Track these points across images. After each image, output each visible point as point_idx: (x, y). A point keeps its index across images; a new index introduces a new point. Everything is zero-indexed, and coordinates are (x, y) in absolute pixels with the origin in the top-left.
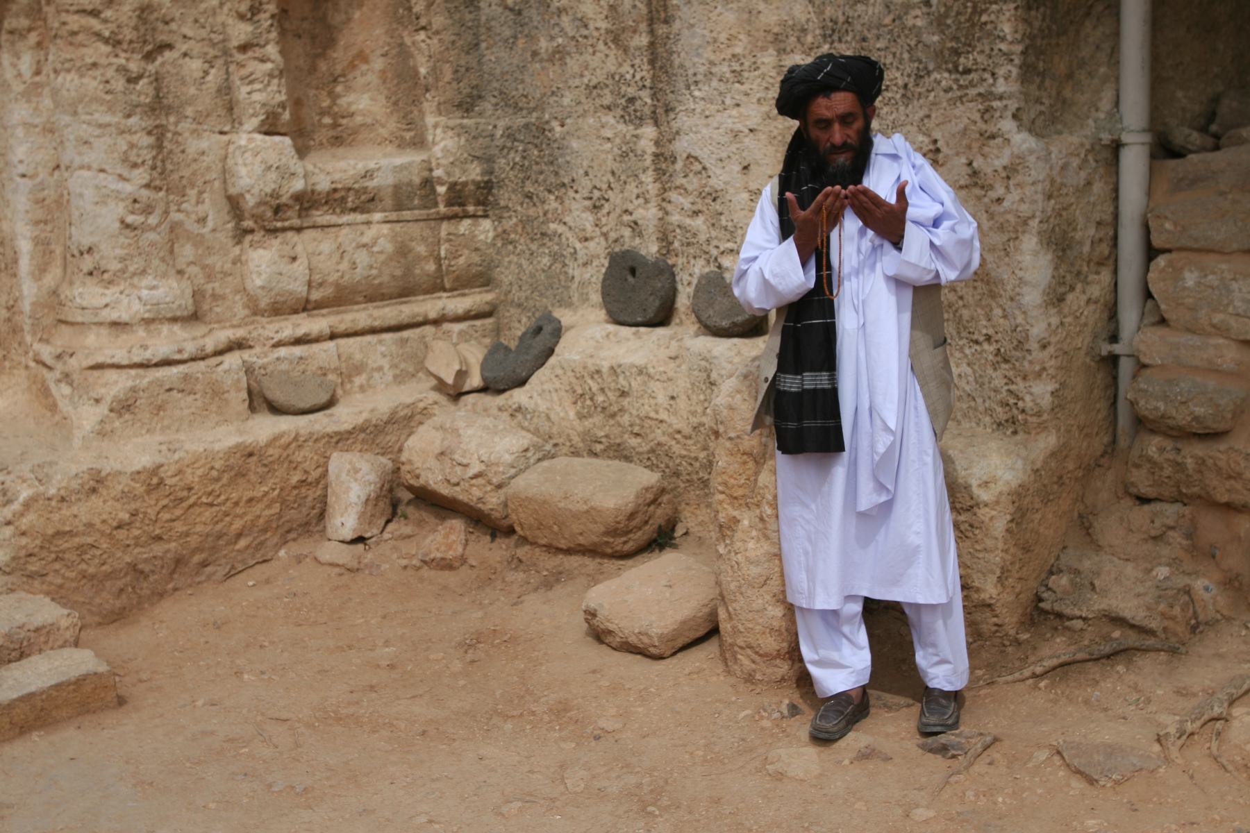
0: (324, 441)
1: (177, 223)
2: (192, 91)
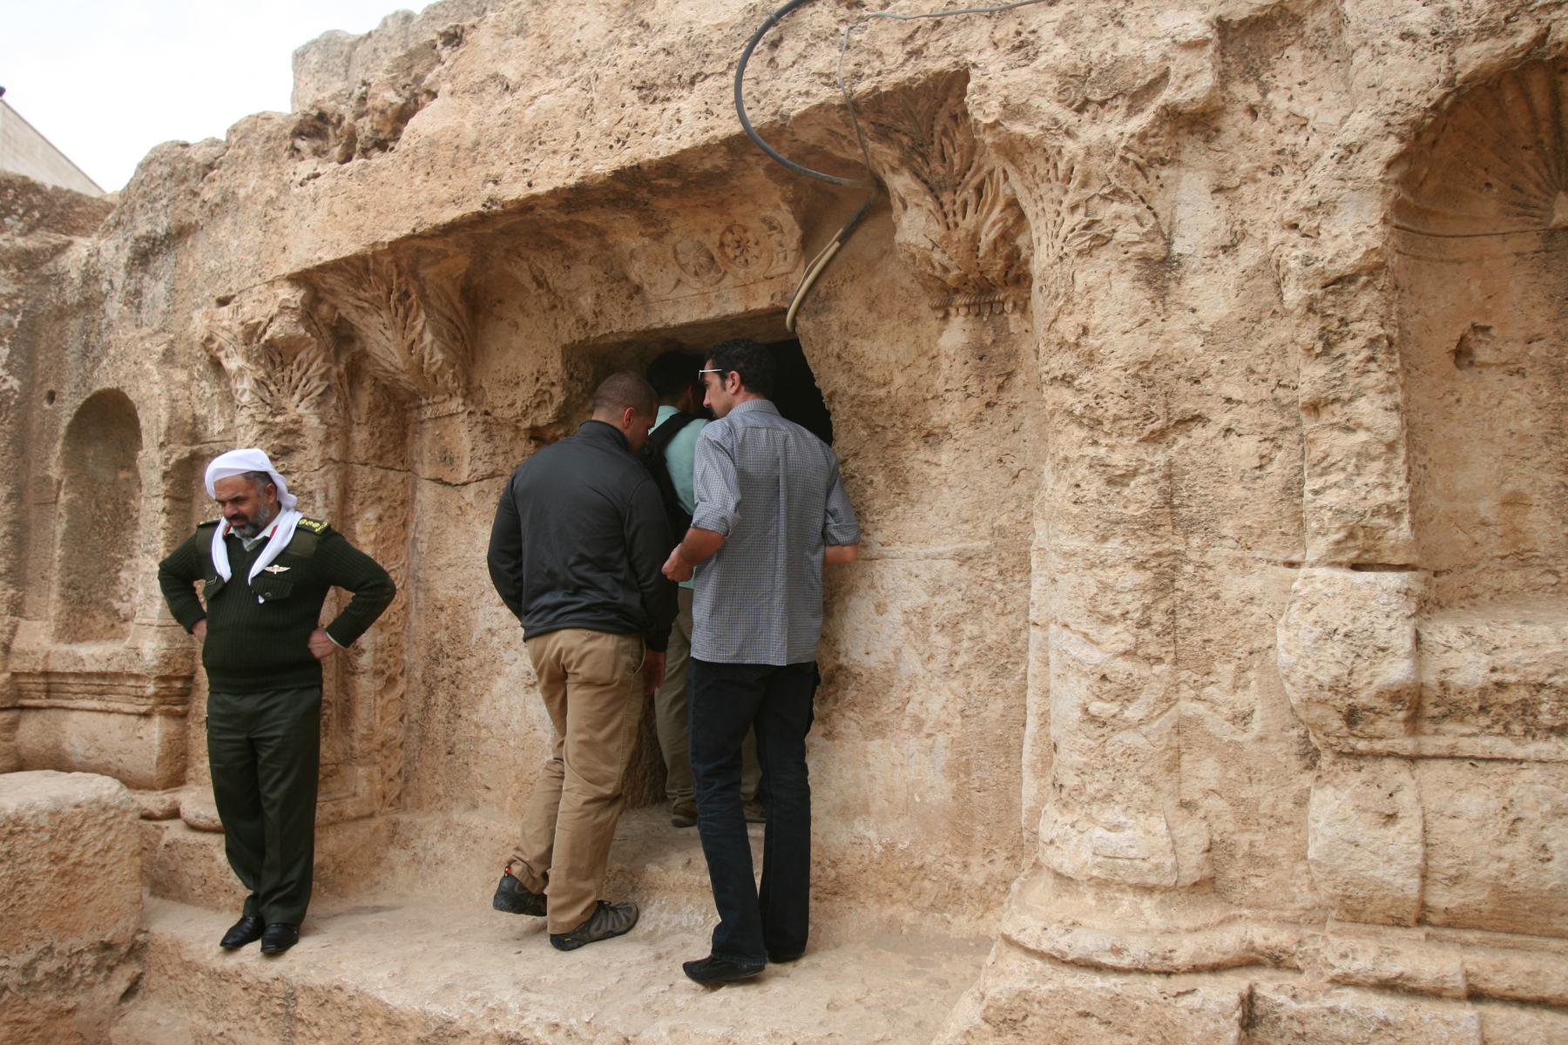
1: (1189, 719)
2: (1237, 491)
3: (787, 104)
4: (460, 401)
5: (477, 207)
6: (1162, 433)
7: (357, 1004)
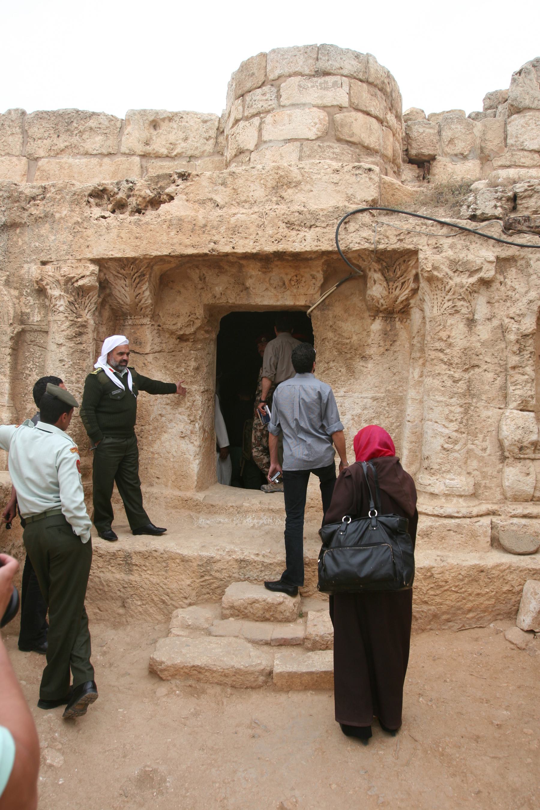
0: (525, 572)
1: (471, 450)
2: (487, 387)
3: (351, 246)
4: (149, 319)
5: (206, 251)
6: (467, 369)
7: (166, 556)
